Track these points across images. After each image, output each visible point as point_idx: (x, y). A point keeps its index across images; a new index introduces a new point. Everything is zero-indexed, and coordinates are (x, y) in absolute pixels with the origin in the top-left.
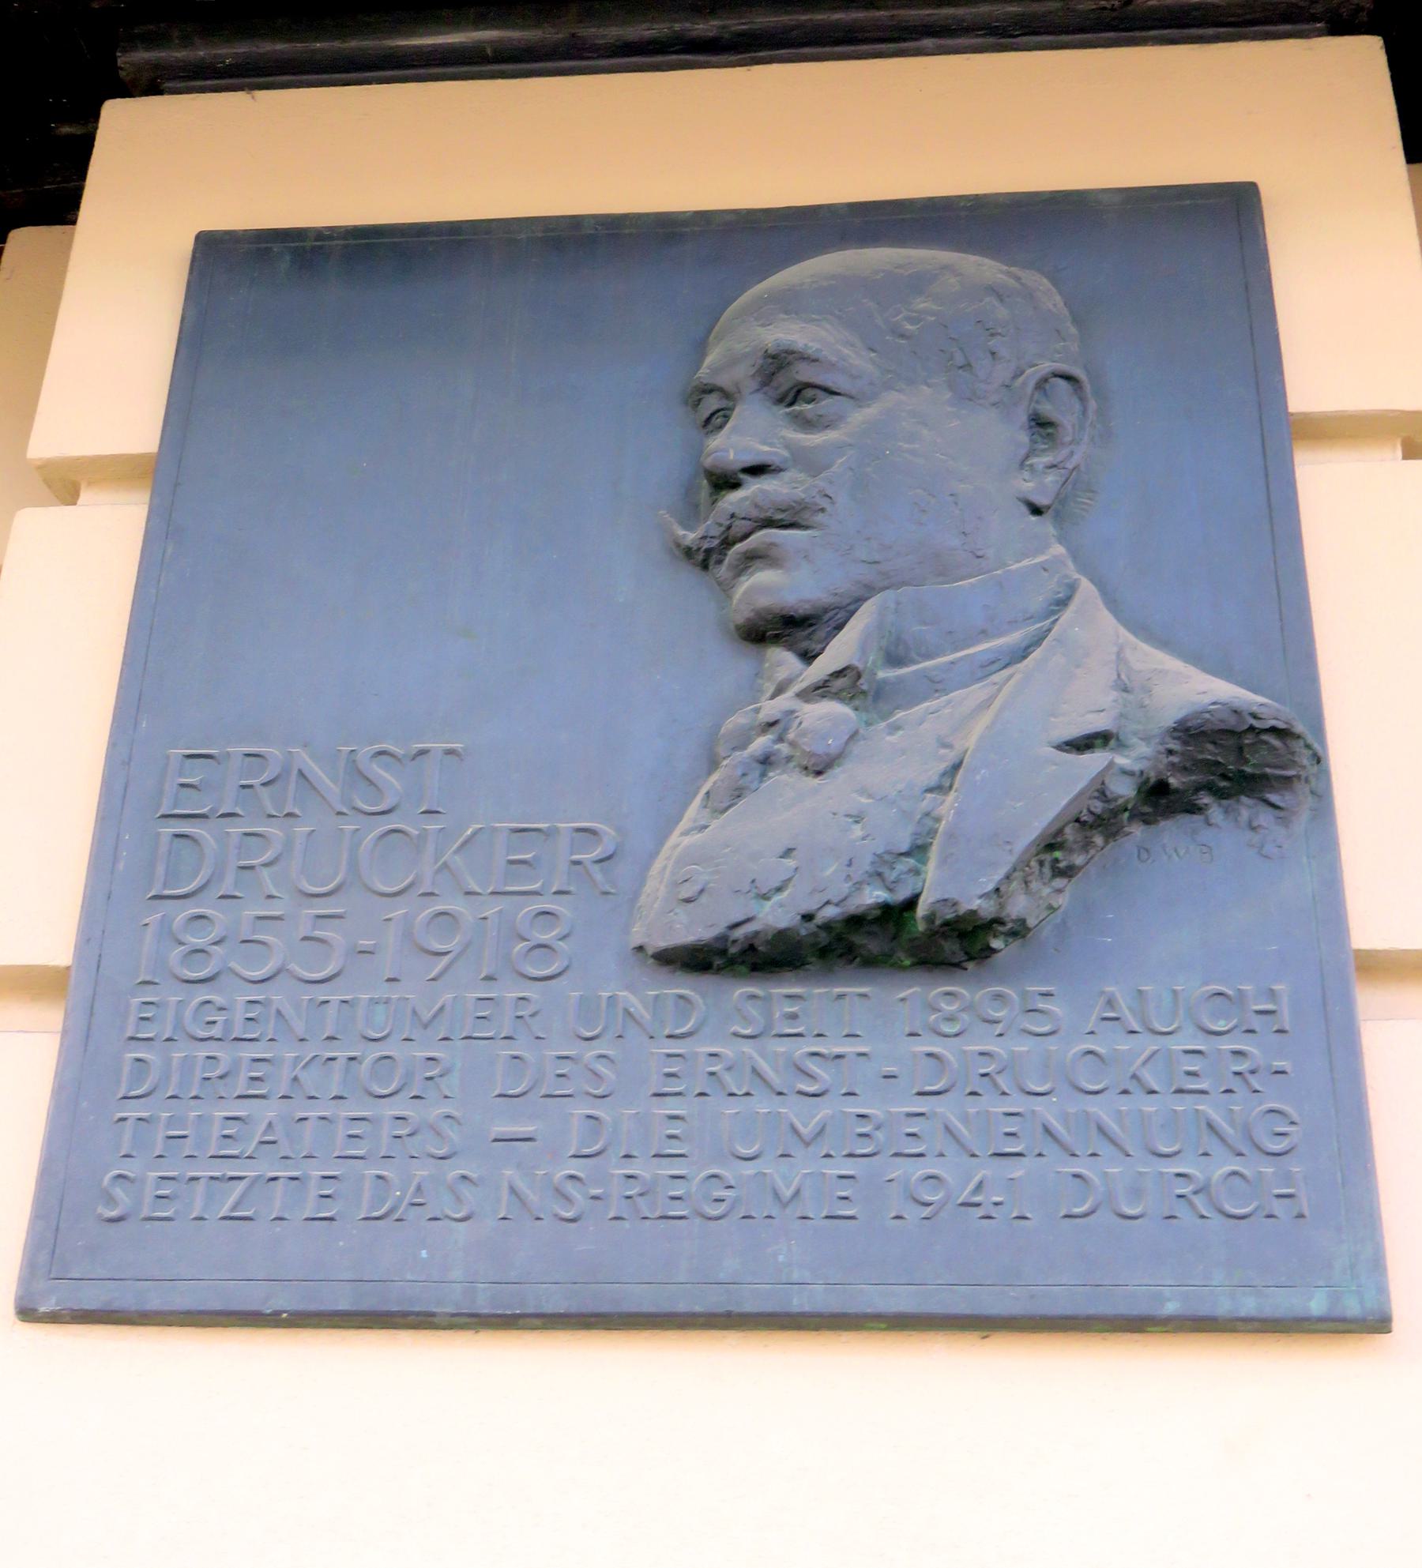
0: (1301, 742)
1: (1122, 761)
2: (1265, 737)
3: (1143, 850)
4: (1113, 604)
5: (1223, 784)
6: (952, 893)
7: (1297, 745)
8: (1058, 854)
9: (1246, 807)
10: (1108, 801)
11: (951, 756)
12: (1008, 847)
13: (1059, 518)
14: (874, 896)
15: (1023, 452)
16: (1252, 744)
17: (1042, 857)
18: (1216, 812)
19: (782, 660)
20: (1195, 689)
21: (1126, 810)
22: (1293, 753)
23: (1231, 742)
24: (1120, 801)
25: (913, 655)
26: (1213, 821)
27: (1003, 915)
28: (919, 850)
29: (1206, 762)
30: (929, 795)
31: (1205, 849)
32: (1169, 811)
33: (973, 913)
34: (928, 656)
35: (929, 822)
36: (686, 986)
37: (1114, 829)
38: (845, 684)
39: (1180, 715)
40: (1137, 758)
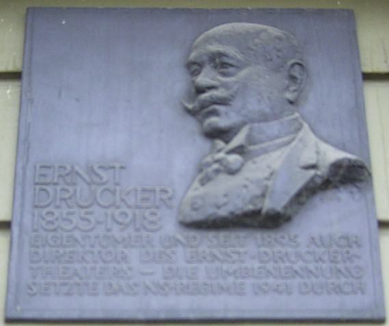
4: (313, 130)
14: (251, 207)
19: (220, 144)
20: (333, 155)
28: (263, 196)
36: (192, 233)
38: (240, 150)
40: (323, 171)
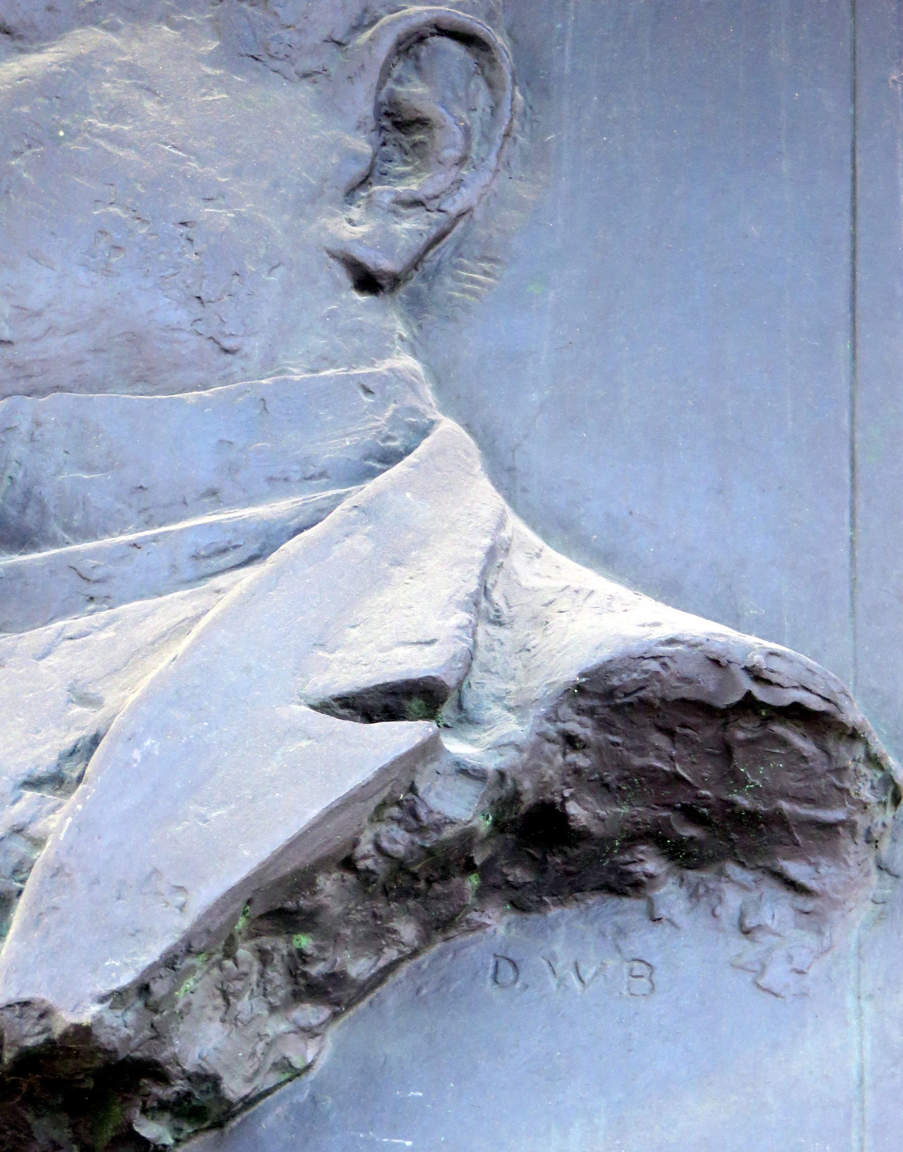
0: (859, 751)
1: (457, 747)
2: (778, 729)
3: (506, 966)
4: (505, 474)
5: (689, 831)
6: (40, 991)
7: (850, 756)
8: (305, 942)
9: (737, 889)
10: (421, 830)
11: (88, 720)
12: (181, 899)
13: (416, 307)
15: (357, 170)
16: (750, 742)
17: (267, 942)
18: (670, 895)
21: (469, 867)
22: (840, 771)
23: (707, 733)
24: (448, 832)
25: (55, 528)
26: (662, 912)
27: (162, 1056)
29: (650, 775)
30: (29, 794)
31: (639, 969)
32: (570, 886)
33: (82, 1033)
34: (86, 533)
35: (19, 846)
37: (443, 909)
39: (590, 659)
40: (495, 740)
